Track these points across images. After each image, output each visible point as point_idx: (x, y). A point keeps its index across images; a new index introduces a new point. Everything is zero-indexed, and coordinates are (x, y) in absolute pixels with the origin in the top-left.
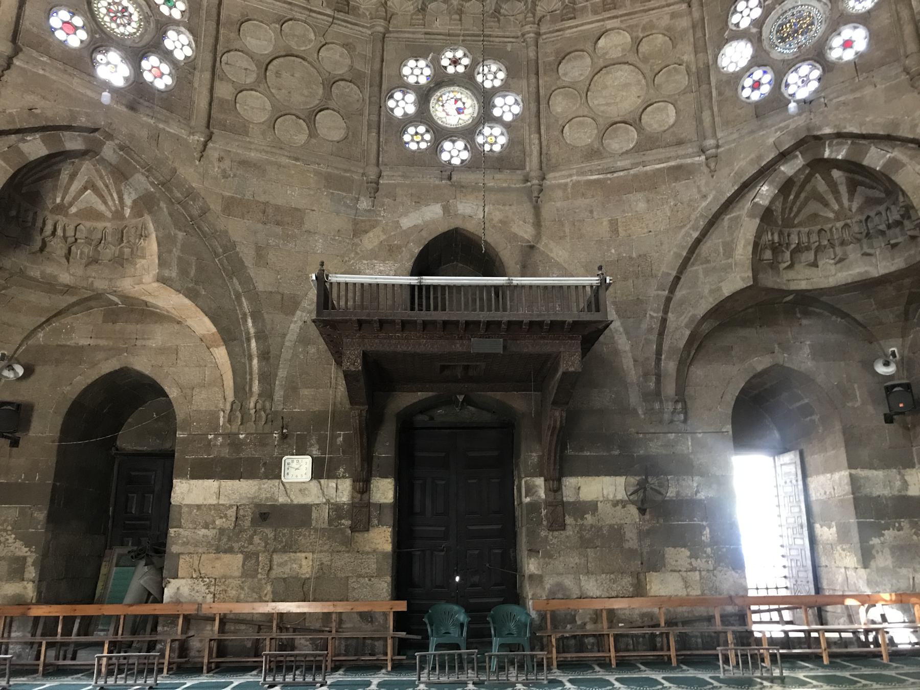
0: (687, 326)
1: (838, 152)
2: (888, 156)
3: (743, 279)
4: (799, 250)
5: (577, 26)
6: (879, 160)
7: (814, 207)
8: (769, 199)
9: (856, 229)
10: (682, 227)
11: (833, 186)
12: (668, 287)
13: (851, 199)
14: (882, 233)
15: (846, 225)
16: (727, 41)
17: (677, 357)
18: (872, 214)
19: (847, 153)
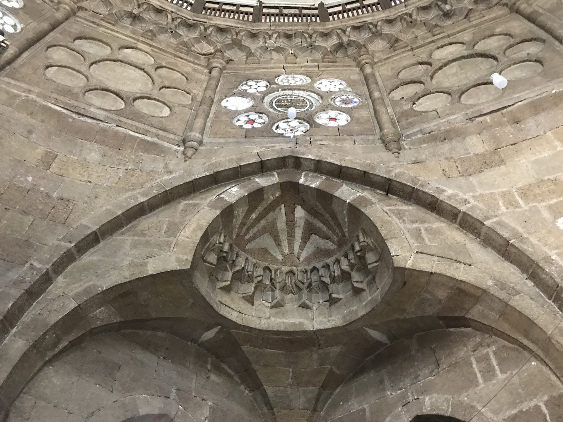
0: (75, 297)
1: (312, 182)
2: (358, 194)
3: (178, 261)
4: (239, 277)
5: (112, 30)
6: (349, 195)
7: (267, 241)
8: (237, 198)
9: (300, 276)
10: (129, 190)
11: (291, 223)
12: (79, 239)
13: (302, 248)
14: (324, 287)
15: (291, 272)
16: (234, 95)
17: (34, 335)
18: (319, 265)
19: (320, 184)
